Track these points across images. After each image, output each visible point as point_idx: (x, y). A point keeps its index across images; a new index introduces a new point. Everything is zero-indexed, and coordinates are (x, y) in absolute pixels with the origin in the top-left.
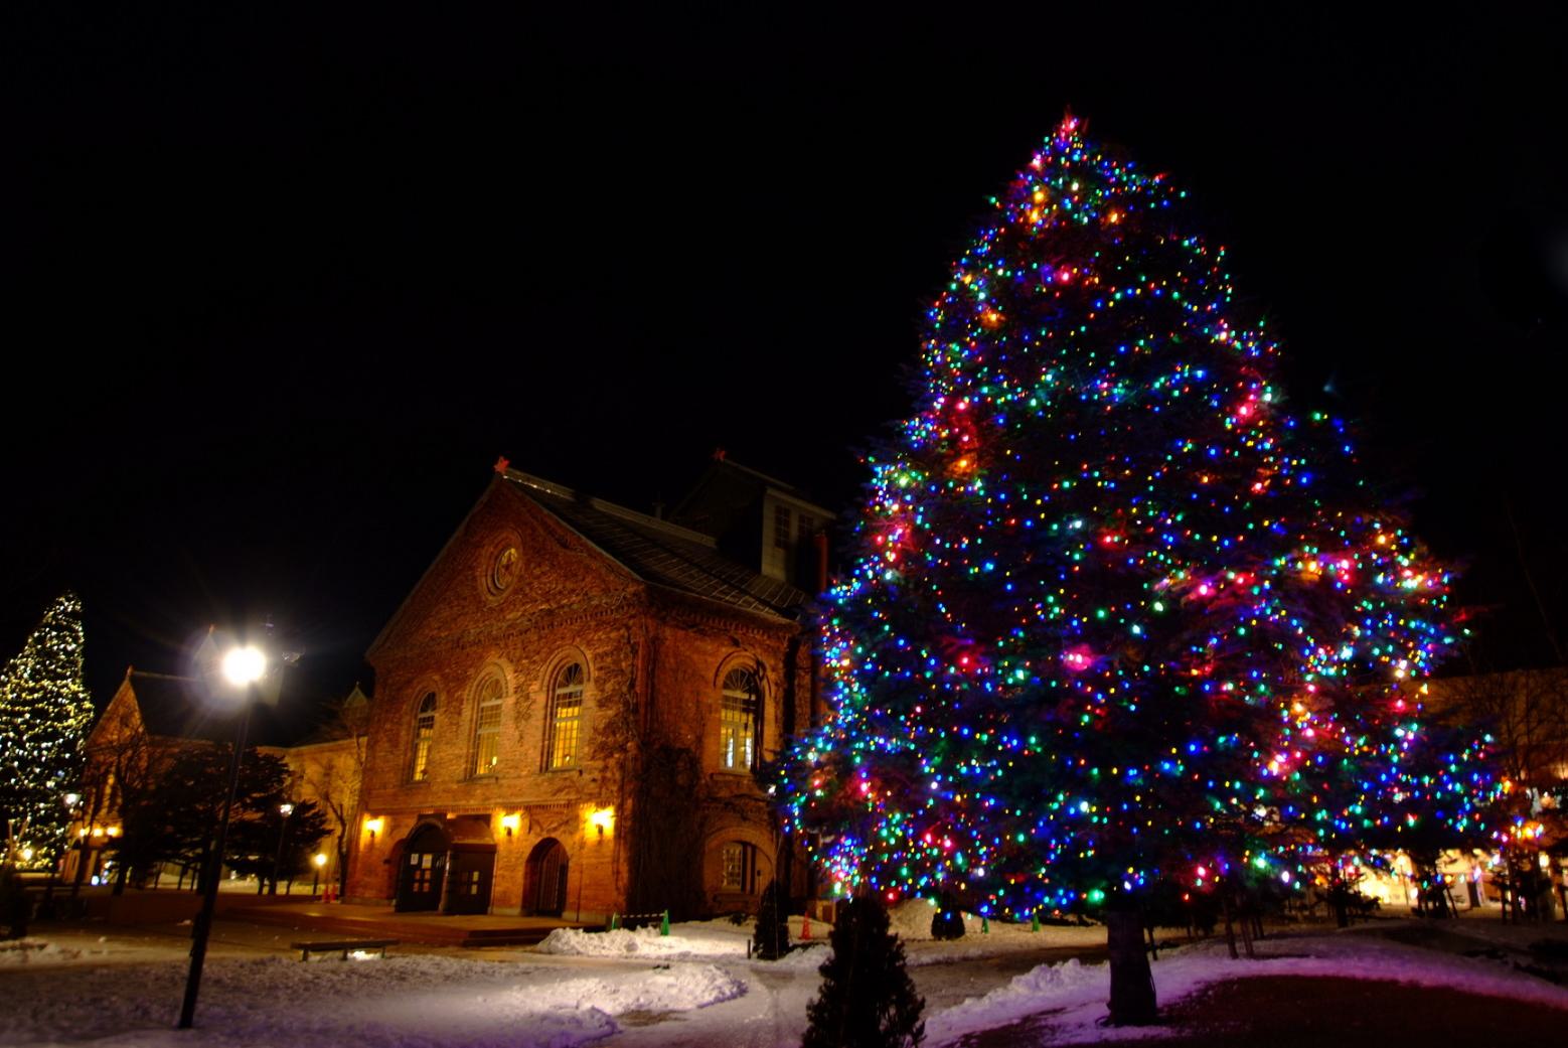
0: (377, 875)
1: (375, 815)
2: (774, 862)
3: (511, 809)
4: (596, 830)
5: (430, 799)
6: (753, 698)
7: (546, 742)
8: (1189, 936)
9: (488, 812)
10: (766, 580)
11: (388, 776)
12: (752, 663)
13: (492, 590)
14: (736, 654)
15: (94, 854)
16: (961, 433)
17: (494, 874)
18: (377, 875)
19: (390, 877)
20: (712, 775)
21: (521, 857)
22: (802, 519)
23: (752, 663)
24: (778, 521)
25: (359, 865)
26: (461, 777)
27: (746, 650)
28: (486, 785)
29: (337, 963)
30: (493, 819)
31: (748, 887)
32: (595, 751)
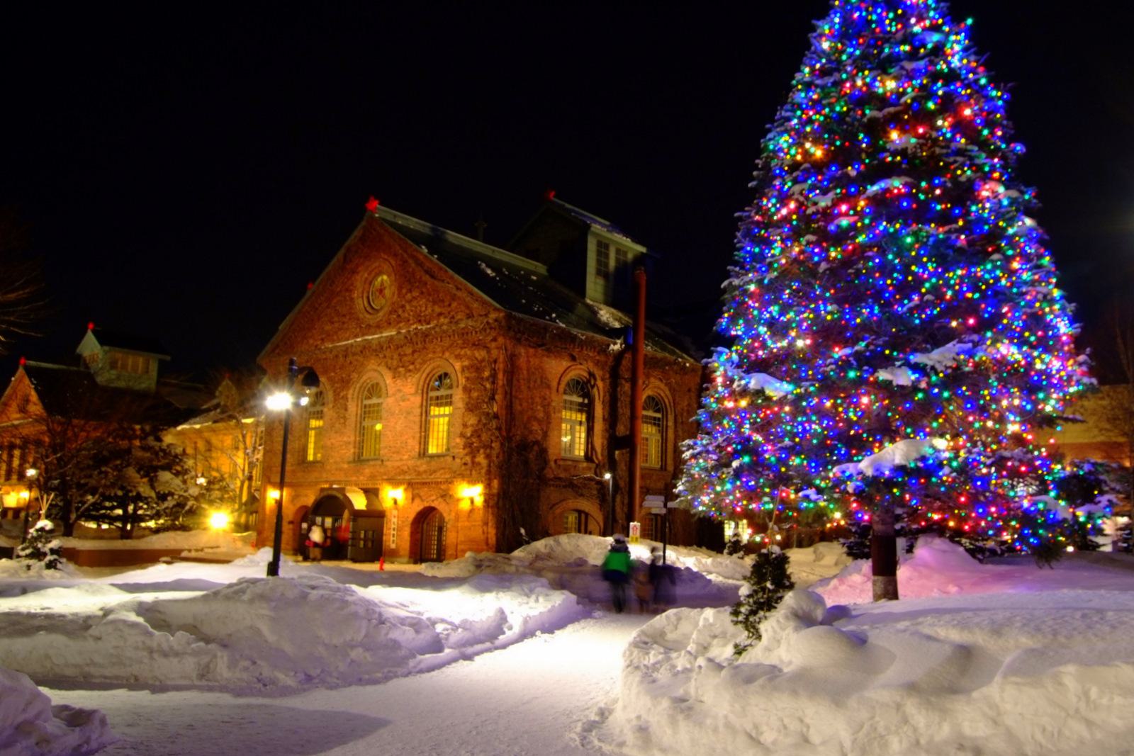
2: (602, 524)
3: (394, 482)
20: (556, 461)
22: (618, 251)
24: (599, 253)
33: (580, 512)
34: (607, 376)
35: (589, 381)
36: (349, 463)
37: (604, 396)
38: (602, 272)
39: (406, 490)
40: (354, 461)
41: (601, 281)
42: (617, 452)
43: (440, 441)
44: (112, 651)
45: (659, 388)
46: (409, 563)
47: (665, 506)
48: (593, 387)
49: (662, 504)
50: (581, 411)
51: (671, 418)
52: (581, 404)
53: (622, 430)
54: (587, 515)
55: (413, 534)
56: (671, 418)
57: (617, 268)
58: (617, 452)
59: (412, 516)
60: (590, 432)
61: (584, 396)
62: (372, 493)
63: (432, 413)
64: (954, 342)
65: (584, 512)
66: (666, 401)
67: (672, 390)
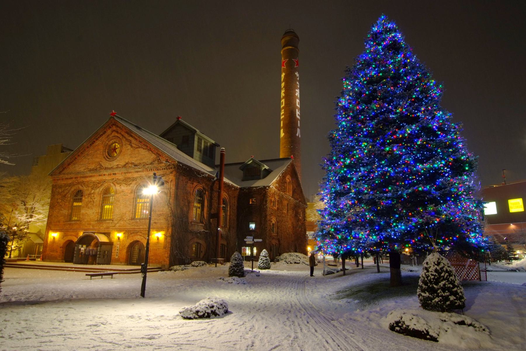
0: (57, 252)
1: (55, 230)
2: (205, 248)
3: (120, 230)
4: (156, 239)
5: (81, 227)
6: (201, 199)
7: (134, 210)
8: (142, 272)
9: (109, 232)
10: (262, 176)
11: (60, 218)
12: (202, 188)
13: (108, 156)
14: (198, 185)
15: (38, 246)
16: (406, 175)
17: (113, 252)
18: (57, 252)
19: (63, 253)
20: (191, 222)
21: (124, 246)
22: (205, 142)
23: (202, 188)
24: (198, 142)
25: (48, 249)
26: (96, 219)
27: (201, 184)
28: (108, 223)
29: (505, 264)
30: (111, 234)
31: (198, 256)
32: (89, 208)
33: (198, 243)
34: (209, 190)
35: (203, 191)
36: (96, 221)
37: (208, 198)
38: (199, 150)
39: (124, 233)
40: (98, 221)
41: (198, 153)
42: (211, 220)
43: (75, 214)
44: (356, 290)
45: (225, 195)
46: (63, 262)
47: (253, 240)
48: (204, 194)
49: (252, 240)
50: (199, 203)
51: (229, 207)
52: (199, 200)
53: (213, 211)
54: (201, 244)
55: (127, 252)
56: (229, 207)
57: (204, 148)
58: (211, 220)
59: (127, 244)
60: (202, 210)
61: (200, 197)
62: (108, 234)
63: (138, 201)
64: (290, 179)
65: (200, 243)
66: (227, 200)
67: (229, 196)
